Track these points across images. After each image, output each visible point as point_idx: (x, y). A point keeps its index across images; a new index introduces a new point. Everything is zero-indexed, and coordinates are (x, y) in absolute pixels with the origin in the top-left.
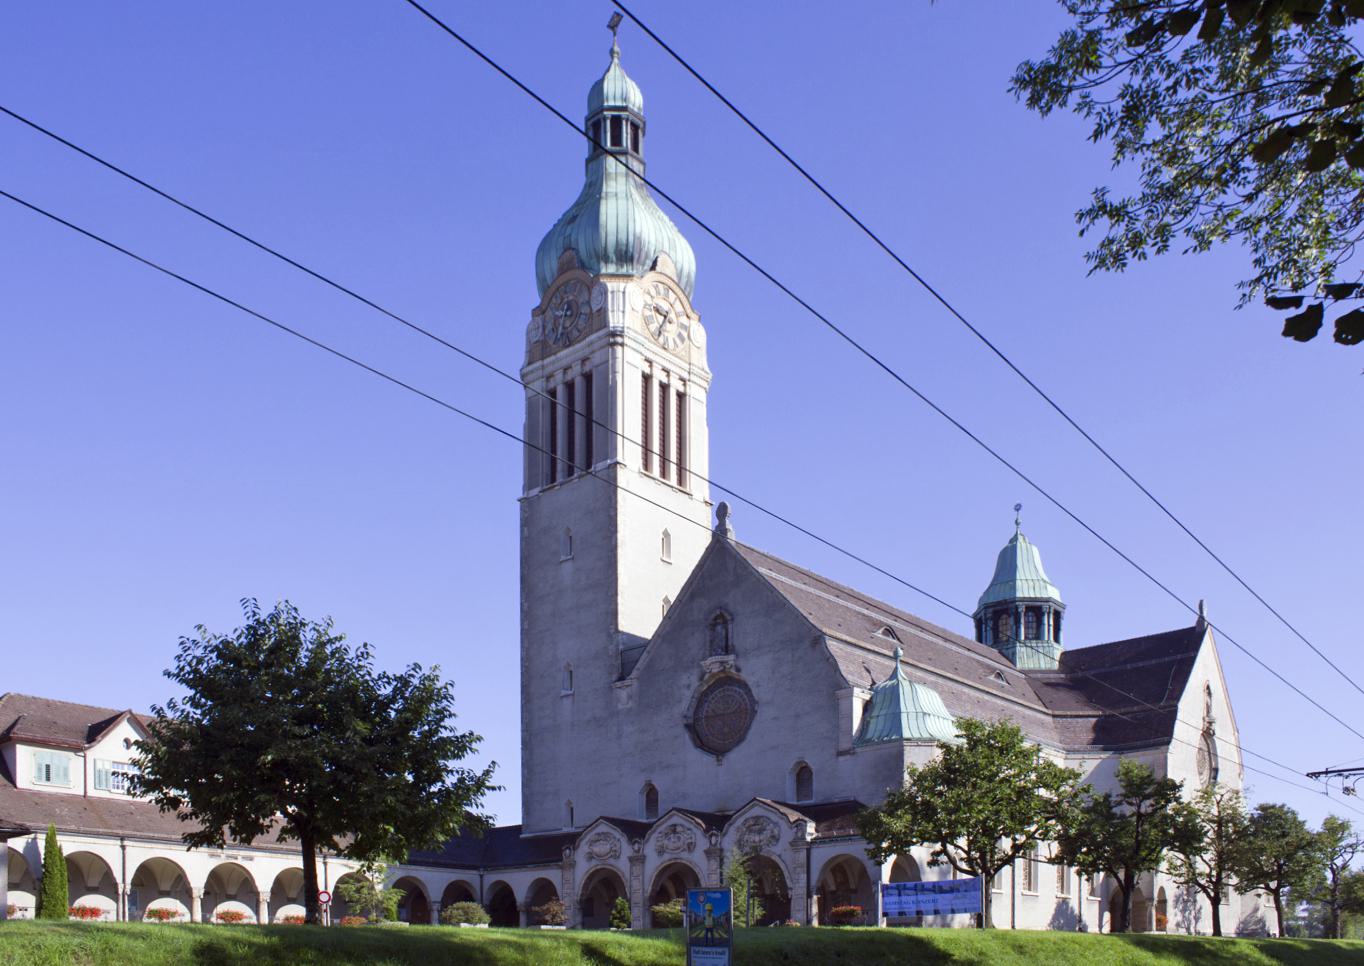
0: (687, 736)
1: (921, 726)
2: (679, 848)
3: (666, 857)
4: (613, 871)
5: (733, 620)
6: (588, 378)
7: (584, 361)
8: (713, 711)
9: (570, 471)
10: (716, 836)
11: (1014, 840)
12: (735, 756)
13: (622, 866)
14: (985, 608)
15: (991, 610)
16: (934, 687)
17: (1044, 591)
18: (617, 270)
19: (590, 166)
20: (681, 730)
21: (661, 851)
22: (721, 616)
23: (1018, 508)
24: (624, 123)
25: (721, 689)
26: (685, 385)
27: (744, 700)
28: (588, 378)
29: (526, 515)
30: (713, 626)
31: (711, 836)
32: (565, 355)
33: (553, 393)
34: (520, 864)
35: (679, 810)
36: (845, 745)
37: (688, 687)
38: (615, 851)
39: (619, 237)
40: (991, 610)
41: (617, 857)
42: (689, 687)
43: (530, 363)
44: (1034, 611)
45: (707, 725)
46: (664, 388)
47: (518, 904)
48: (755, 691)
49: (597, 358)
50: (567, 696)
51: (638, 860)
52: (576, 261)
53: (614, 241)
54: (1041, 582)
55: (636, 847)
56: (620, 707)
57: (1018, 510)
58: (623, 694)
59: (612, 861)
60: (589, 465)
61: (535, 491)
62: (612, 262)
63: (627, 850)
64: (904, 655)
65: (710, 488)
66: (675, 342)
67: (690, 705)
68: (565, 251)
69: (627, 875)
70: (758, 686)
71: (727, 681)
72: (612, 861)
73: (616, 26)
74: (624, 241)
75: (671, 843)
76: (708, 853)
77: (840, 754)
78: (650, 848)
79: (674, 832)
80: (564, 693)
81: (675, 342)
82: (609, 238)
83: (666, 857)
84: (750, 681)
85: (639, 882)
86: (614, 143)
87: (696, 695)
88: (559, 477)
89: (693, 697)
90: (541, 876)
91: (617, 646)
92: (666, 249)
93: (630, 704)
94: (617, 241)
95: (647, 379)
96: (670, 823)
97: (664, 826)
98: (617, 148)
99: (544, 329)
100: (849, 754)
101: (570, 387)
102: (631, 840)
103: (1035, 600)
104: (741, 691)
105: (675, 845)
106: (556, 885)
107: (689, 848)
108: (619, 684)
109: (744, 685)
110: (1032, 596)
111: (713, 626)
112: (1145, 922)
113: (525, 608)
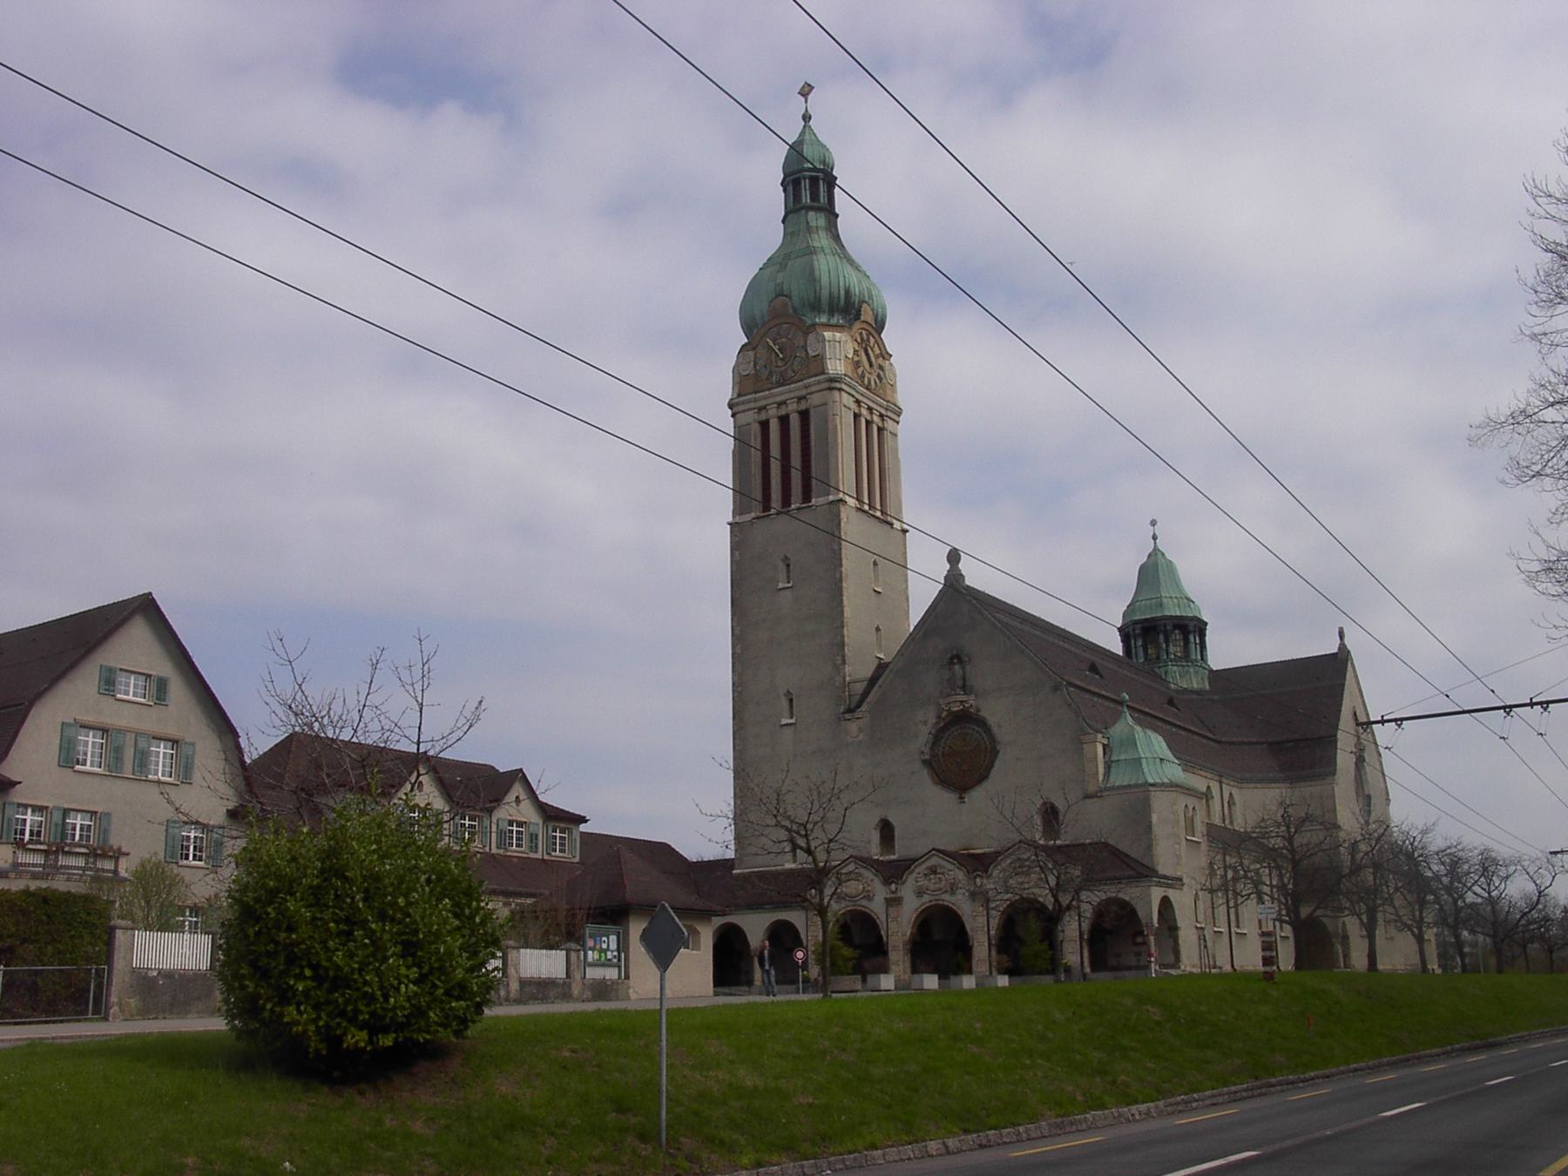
0: (925, 772)
1: (1160, 771)
2: (940, 889)
3: (926, 898)
4: (867, 913)
5: (970, 661)
6: (804, 415)
7: (800, 399)
8: (950, 747)
9: (786, 501)
10: (981, 877)
11: (1465, 902)
12: (977, 795)
13: (877, 907)
14: (1134, 624)
15: (1139, 626)
16: (1155, 730)
17: (1185, 611)
18: (829, 319)
19: (790, 216)
20: (918, 765)
21: (920, 893)
22: (958, 657)
23: (1153, 523)
24: (821, 182)
25: (958, 727)
26: (883, 420)
27: (983, 739)
28: (804, 415)
29: (737, 539)
30: (951, 662)
31: (975, 878)
32: (781, 393)
33: (765, 425)
34: (756, 905)
35: (939, 851)
36: (1091, 789)
37: (924, 723)
38: (868, 891)
39: (832, 290)
40: (1139, 626)
41: (870, 898)
42: (925, 723)
43: (739, 395)
44: (1180, 629)
45: (944, 761)
46: (868, 423)
47: (752, 947)
48: (995, 730)
49: (815, 399)
50: (787, 725)
51: (893, 902)
52: (790, 307)
53: (828, 291)
54: (1186, 601)
55: (893, 886)
56: (849, 739)
57: (1154, 525)
58: (853, 727)
59: (864, 902)
60: (807, 497)
61: (747, 517)
62: (824, 312)
63: (881, 892)
64: (1130, 701)
65: (828, 480)
66: (876, 383)
67: (927, 742)
68: (777, 296)
69: (883, 917)
70: (999, 726)
71: (965, 718)
72: (864, 902)
73: (808, 94)
74: (836, 295)
75: (931, 883)
76: (973, 895)
77: (1088, 796)
78: (907, 891)
79: (935, 872)
80: (784, 721)
81: (876, 383)
82: (823, 291)
83: (926, 898)
84: (991, 721)
85: (899, 929)
86: (813, 199)
87: (933, 732)
88: (776, 503)
89: (930, 733)
90: (780, 918)
91: (845, 678)
92: (867, 299)
93: (861, 737)
94: (830, 294)
95: (857, 416)
96: (928, 864)
97: (924, 866)
98: (816, 204)
99: (755, 365)
100: (1097, 797)
101: (784, 421)
102: (887, 881)
103: (1181, 617)
104: (980, 729)
105: (937, 886)
106: (800, 930)
107: (952, 889)
108: (848, 716)
109: (982, 723)
110: (1178, 614)
111: (951, 662)
112: (106, 1041)
113: (736, 632)
